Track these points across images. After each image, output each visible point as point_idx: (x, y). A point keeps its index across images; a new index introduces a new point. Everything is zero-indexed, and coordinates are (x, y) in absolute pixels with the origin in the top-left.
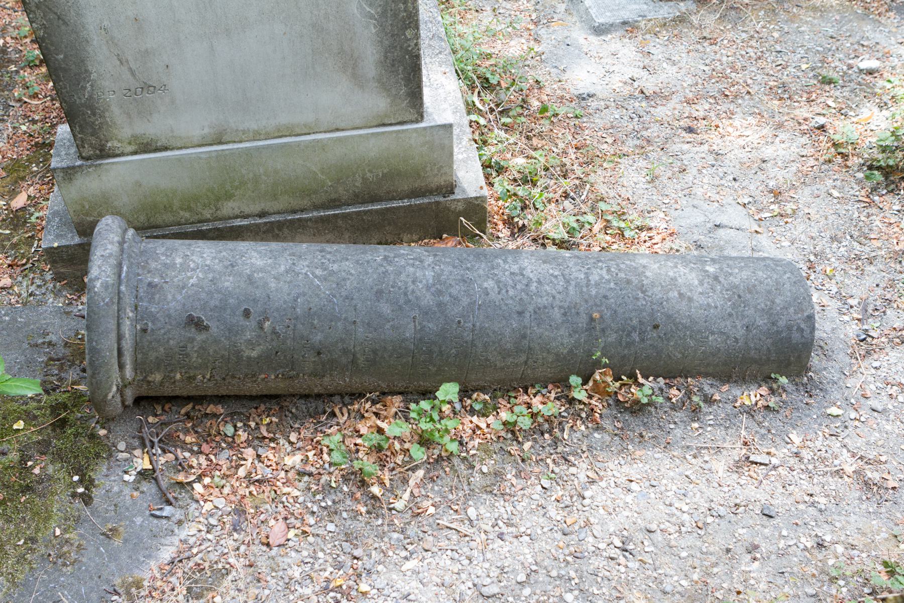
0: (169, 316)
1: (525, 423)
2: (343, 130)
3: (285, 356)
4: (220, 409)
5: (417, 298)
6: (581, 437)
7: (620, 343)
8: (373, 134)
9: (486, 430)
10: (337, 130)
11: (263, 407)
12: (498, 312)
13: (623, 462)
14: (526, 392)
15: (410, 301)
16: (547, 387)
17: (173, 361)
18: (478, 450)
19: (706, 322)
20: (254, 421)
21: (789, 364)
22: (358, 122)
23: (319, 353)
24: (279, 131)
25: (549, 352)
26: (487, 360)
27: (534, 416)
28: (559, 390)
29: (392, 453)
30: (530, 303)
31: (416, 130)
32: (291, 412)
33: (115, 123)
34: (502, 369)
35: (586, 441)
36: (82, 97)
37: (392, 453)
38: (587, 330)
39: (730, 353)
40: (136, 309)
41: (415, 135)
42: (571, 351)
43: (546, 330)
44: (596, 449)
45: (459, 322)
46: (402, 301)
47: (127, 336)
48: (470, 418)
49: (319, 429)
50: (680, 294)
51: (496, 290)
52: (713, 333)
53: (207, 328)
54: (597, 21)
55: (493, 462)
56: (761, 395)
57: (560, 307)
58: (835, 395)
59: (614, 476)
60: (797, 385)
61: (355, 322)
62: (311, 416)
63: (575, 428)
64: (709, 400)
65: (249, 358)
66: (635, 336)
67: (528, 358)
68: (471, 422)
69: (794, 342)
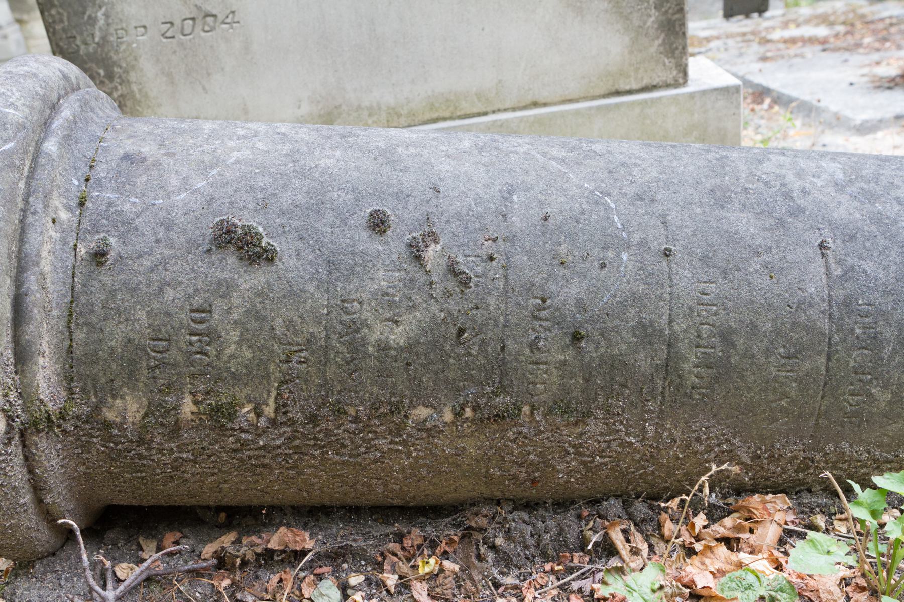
0: (168, 226)
2: (545, 105)
3: (483, 343)
4: (307, 541)
8: (598, 108)
10: (535, 105)
11: (415, 536)
15: (802, 210)
17: (174, 355)
20: (394, 572)
23: (576, 337)
31: (675, 98)
32: (493, 547)
33: (146, 96)
36: (89, 39)
40: (82, 204)
47: (46, 266)
49: (575, 586)
53: (267, 257)
61: (667, 254)
62: (546, 558)
65: (383, 347)
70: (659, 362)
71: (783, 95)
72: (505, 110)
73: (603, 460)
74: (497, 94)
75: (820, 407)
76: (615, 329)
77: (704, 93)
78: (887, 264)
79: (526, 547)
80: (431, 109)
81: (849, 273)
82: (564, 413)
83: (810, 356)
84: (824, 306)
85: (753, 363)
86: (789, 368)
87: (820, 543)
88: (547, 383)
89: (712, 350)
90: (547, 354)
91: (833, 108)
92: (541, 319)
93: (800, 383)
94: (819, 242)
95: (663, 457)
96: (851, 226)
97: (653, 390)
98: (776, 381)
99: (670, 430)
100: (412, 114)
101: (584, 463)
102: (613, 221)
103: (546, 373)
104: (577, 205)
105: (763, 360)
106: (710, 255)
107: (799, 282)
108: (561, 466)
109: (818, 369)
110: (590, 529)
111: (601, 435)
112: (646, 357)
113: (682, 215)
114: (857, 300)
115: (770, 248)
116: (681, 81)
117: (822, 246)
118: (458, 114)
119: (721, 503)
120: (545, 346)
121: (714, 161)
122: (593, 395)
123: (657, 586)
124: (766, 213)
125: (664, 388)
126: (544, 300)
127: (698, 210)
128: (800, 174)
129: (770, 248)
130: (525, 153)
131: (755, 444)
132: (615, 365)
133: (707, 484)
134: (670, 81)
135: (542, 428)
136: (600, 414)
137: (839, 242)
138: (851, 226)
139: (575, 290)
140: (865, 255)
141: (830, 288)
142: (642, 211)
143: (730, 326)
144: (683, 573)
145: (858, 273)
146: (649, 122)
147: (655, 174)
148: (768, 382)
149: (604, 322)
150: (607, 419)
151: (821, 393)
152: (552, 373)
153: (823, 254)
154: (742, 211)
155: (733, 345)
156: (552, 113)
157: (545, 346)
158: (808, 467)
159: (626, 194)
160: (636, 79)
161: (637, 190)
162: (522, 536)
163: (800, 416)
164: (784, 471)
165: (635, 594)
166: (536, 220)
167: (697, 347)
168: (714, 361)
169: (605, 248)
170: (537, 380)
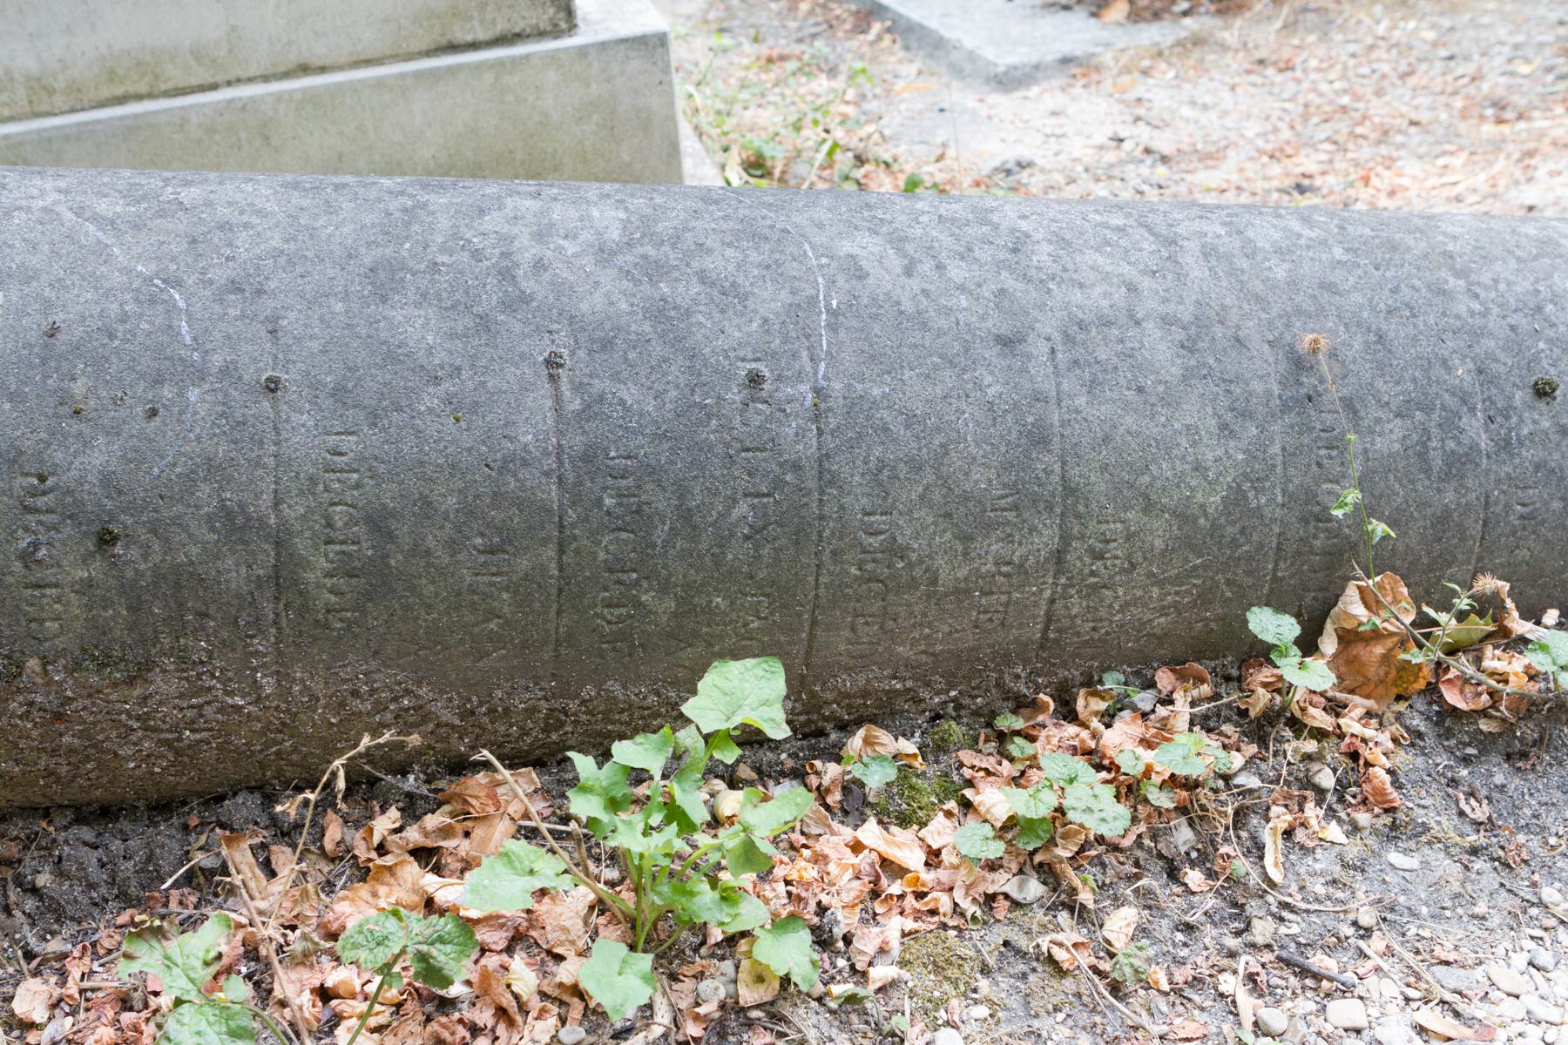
1: (1099, 811)
2: (323, 70)
5: (558, 287)
6: (1337, 870)
7: (1423, 456)
8: (418, 75)
9: (928, 877)
10: (305, 69)
12: (916, 337)
13: (1545, 958)
14: (1068, 713)
15: (525, 299)
16: (1150, 684)
18: (903, 963)
22: (369, 39)
23: (106, 539)
24: (112, 76)
25: (1148, 507)
26: (895, 550)
27: (1130, 791)
28: (1206, 689)
29: (501, 1012)
30: (1042, 307)
31: (553, 56)
32: (34, 891)
34: (961, 592)
35: (1361, 887)
37: (501, 1012)
38: (1285, 408)
41: (553, 76)
42: (1236, 498)
43: (1126, 407)
44: (1415, 915)
45: (755, 380)
46: (489, 300)
48: (847, 833)
51: (895, 263)
54: (1000, 61)
55: (982, 1011)
57: (1167, 321)
59: (1531, 1018)
62: (126, 900)
63: (1300, 835)
66: (1475, 429)
67: (1066, 539)
68: (857, 847)
70: (261, 572)
71: (901, 16)
72: (251, 80)
73: (198, 736)
74: (230, 51)
75: (557, 628)
76: (177, 521)
77: (603, 46)
78: (661, 388)
79: (92, 886)
80: (111, 80)
81: (593, 407)
82: (104, 665)
83: (527, 548)
84: (550, 463)
85: (429, 565)
86: (494, 569)
87: (518, 857)
88: (63, 619)
89: (355, 548)
90: (54, 570)
91: (969, 43)
92: (38, 511)
93: (516, 592)
94: (546, 354)
95: (305, 724)
96: (608, 325)
97: (258, 619)
98: (473, 592)
99: (302, 681)
100: (74, 88)
101: (168, 743)
102: (179, 333)
103: (58, 601)
104: (115, 306)
105: (446, 560)
106: (350, 385)
107: (506, 425)
108: (126, 751)
109: (544, 569)
110: (201, 848)
111: (181, 696)
112: (237, 565)
113: (308, 317)
114: (606, 450)
115: (459, 369)
116: (563, 25)
117: (553, 363)
118: (163, 87)
119: (424, 790)
120: (50, 557)
121: (397, 214)
122: (150, 633)
123: (213, 954)
124: (461, 308)
125: (277, 615)
126: (42, 479)
127: (339, 307)
128: (540, 236)
129: (459, 369)
130: (44, 210)
131: (458, 693)
132: (180, 582)
133: (341, 773)
134: (544, 25)
135: (69, 693)
136: (169, 663)
137: (582, 353)
138: (608, 325)
139: (100, 457)
140: (625, 374)
141: (560, 433)
142: (233, 312)
143: (384, 506)
144: (331, 916)
145: (610, 404)
146: (511, 98)
147: (276, 242)
148: (460, 594)
149: (155, 510)
150: (184, 671)
151: (555, 606)
152: (69, 602)
153: (551, 376)
154: (418, 305)
155: (392, 537)
156: (335, 84)
157: (50, 557)
158: (563, 724)
159: (211, 282)
160: (482, 22)
161: (234, 274)
162: (82, 867)
163: (524, 645)
164: (525, 732)
165: (176, 971)
166: (33, 337)
167: (327, 543)
168: (359, 565)
169: (159, 381)
170: (44, 615)
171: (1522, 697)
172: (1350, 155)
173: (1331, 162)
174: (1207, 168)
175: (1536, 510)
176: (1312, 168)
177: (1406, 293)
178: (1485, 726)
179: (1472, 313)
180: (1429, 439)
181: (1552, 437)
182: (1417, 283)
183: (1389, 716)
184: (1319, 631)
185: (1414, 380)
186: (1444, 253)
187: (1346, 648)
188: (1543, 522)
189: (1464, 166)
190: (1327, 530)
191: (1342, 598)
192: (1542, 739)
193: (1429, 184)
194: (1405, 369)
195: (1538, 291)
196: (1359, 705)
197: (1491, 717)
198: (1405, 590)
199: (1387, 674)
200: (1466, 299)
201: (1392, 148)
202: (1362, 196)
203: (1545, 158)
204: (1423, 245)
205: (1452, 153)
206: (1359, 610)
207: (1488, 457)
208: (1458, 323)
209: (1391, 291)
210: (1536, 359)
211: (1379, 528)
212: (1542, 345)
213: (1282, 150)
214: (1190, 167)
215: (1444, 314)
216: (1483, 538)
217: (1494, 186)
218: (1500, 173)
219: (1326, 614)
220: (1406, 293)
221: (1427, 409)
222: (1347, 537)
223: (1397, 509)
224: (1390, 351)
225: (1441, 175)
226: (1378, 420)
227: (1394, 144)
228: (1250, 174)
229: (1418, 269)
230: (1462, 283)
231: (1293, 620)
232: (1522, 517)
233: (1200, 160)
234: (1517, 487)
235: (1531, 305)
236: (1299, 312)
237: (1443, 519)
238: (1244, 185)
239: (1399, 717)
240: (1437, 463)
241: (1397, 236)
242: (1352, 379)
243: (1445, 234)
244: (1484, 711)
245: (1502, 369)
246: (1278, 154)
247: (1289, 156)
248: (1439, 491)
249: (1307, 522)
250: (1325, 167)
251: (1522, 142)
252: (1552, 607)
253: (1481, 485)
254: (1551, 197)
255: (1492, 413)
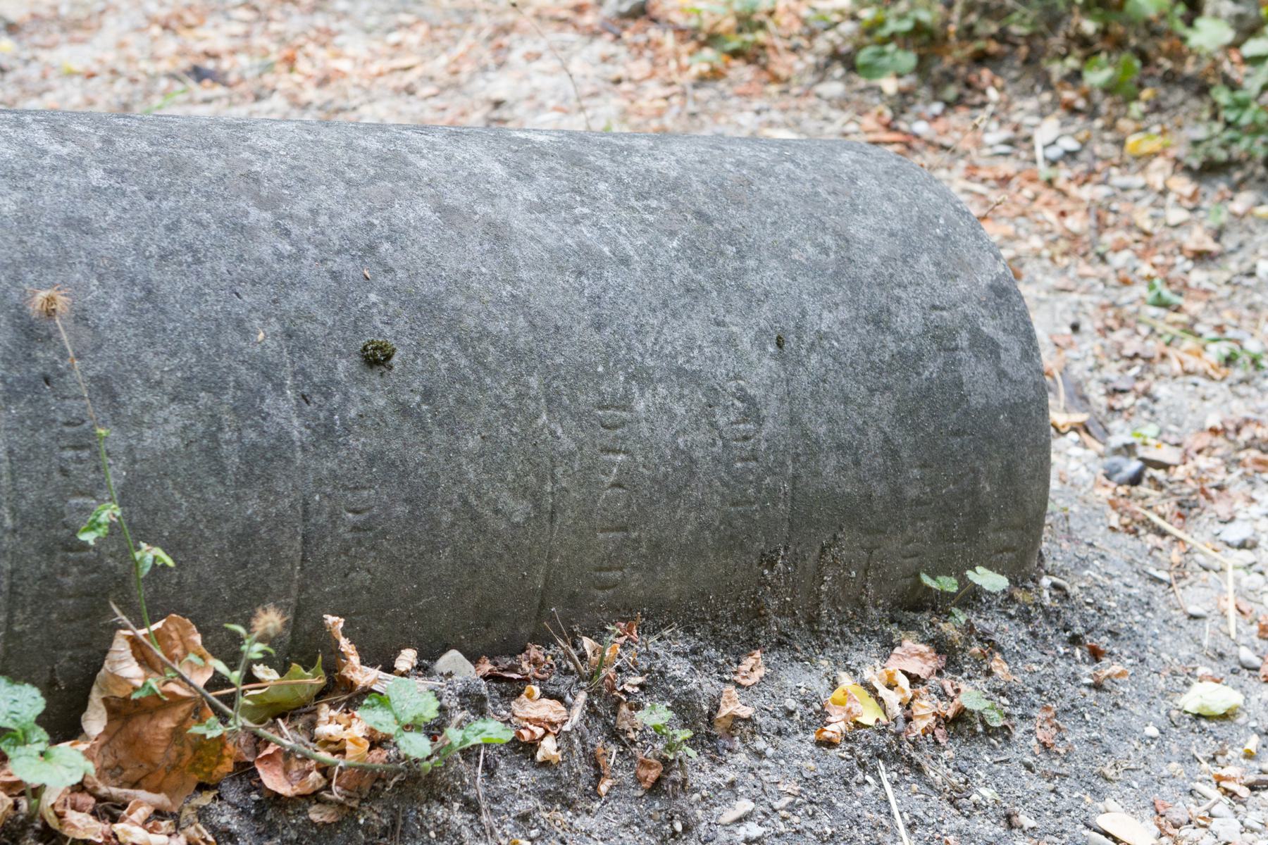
7: (212, 453)
19: (599, 327)
21: (979, 517)
39: (739, 478)
50: (445, 211)
52: (643, 378)
56: (914, 680)
58: (1175, 649)
60: (1026, 617)
64: (711, 732)
66: (284, 413)
69: (976, 401)
171: (362, 770)
172: (274, 27)
173: (247, 35)
174: (73, 41)
175: (373, 517)
176: (219, 42)
177: (188, 231)
178: (316, 815)
179: (280, 257)
180: (220, 429)
181: (389, 418)
182: (205, 217)
183: (188, 813)
184: (82, 705)
185: (197, 349)
186: (247, 175)
187: (124, 725)
188: (384, 533)
189: (422, 44)
190: (81, 561)
191: (109, 656)
192: (394, 825)
193: (374, 69)
194: (183, 335)
195: (372, 225)
196: (144, 801)
197: (324, 802)
198: (197, 638)
199: (180, 755)
200: (272, 237)
201: (331, 18)
202: (280, 86)
203: (524, 34)
204: (219, 163)
205: (408, 27)
206: (131, 670)
207: (304, 449)
208: (260, 271)
209: (168, 228)
210: (365, 316)
211: (149, 554)
212: (373, 297)
213: (180, 18)
214: (49, 41)
215: (240, 258)
216: (304, 560)
217: (455, 73)
218: (463, 56)
219: (90, 680)
220: (188, 231)
221: (216, 388)
222: (112, 570)
223: (181, 526)
224: (163, 311)
225: (392, 57)
226: (146, 407)
227: (334, 12)
228: (133, 51)
229: (208, 196)
230: (268, 215)
231: (35, 692)
232: (355, 528)
233: (64, 30)
234: (346, 488)
235: (361, 244)
236: (33, 259)
237: (246, 536)
238: (121, 67)
239: (202, 813)
240: (233, 461)
241: (185, 153)
242: (108, 351)
243: (252, 149)
244: (315, 793)
245: (319, 331)
246: (174, 23)
247: (190, 27)
248: (238, 498)
249: (51, 553)
250: (238, 43)
251: (499, 13)
252: (409, 645)
253: (295, 488)
254: (526, 88)
255: (306, 390)
